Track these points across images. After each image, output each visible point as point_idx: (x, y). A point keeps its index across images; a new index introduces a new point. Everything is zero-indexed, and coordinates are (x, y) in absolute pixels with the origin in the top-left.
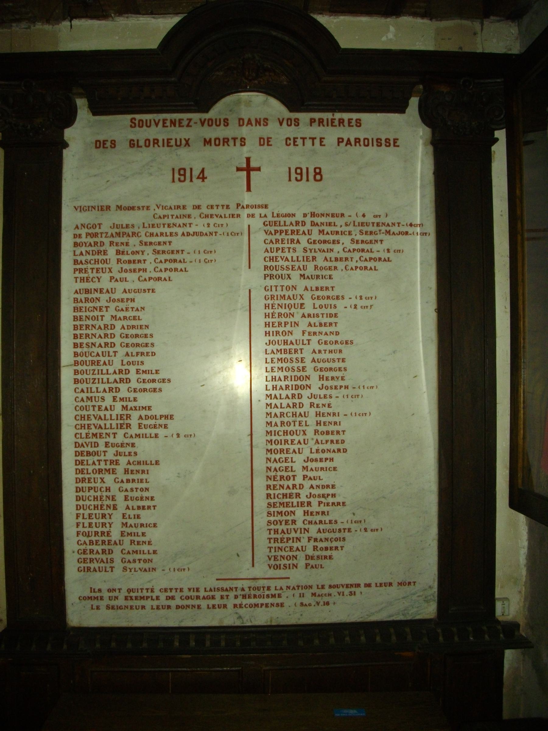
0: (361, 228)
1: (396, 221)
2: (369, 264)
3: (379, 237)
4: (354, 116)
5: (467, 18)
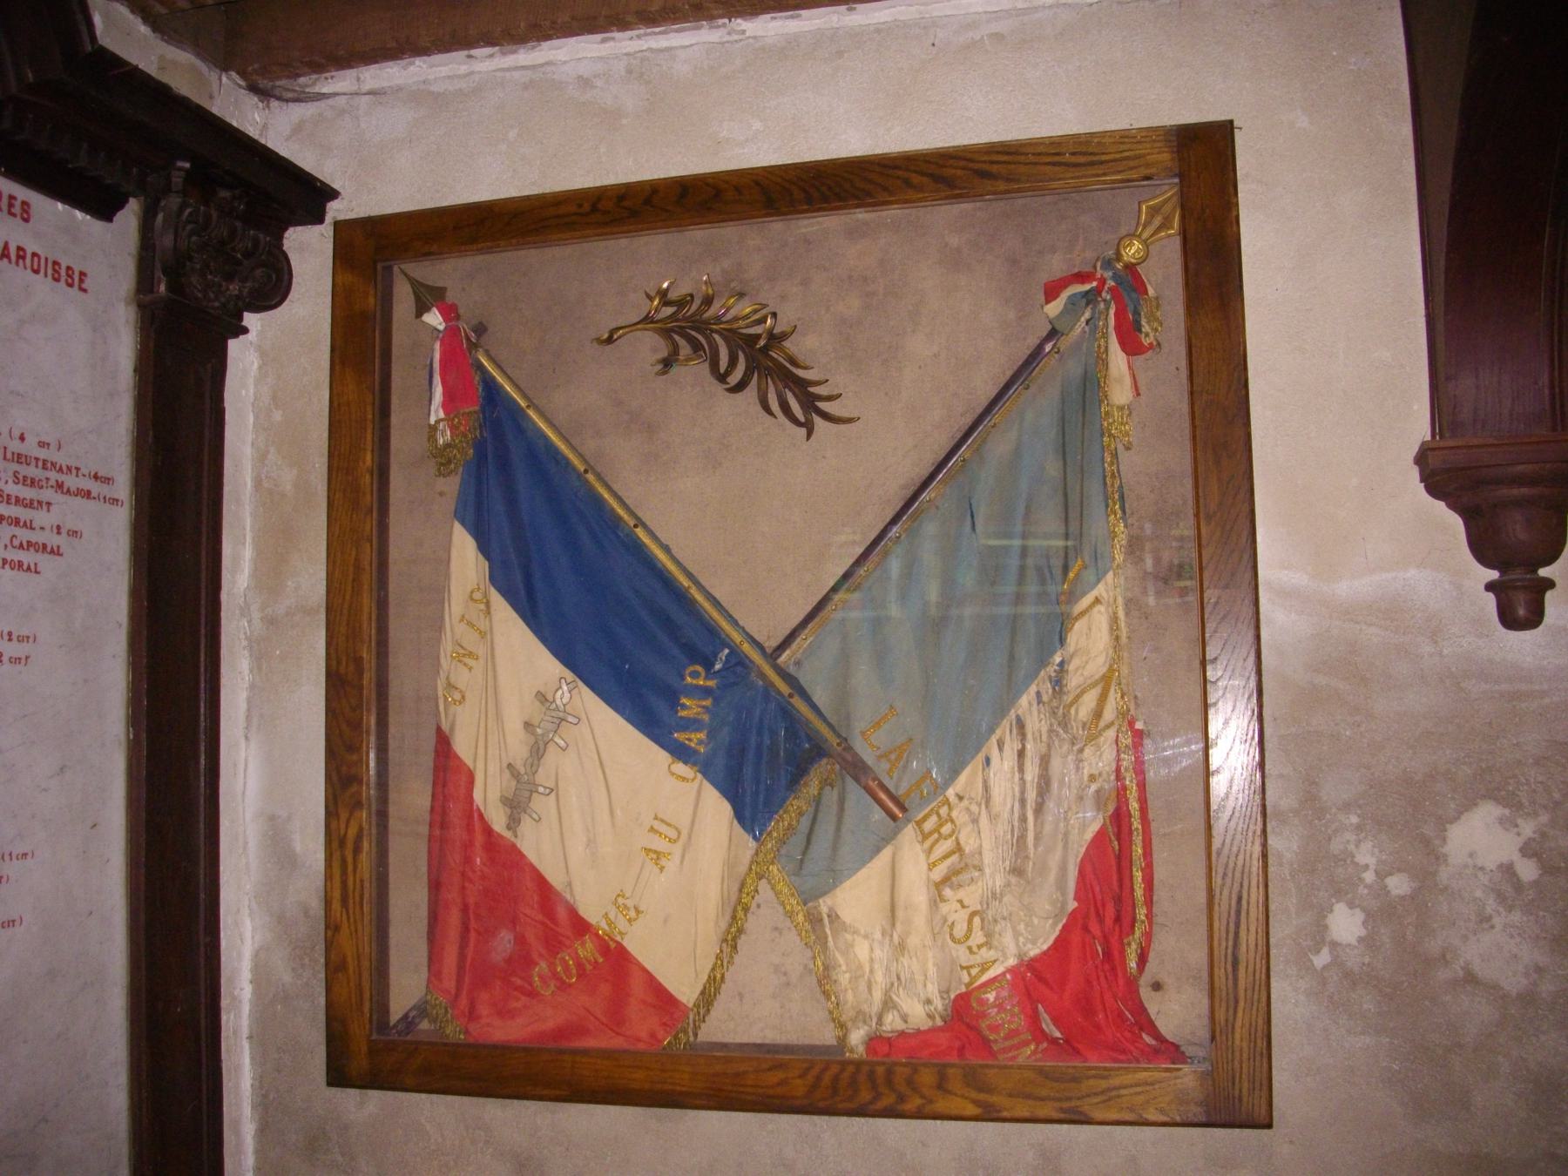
0: (15, 467)
1: (74, 464)
2: (27, 557)
3: (48, 494)
4: (22, 193)
5: (204, 59)
